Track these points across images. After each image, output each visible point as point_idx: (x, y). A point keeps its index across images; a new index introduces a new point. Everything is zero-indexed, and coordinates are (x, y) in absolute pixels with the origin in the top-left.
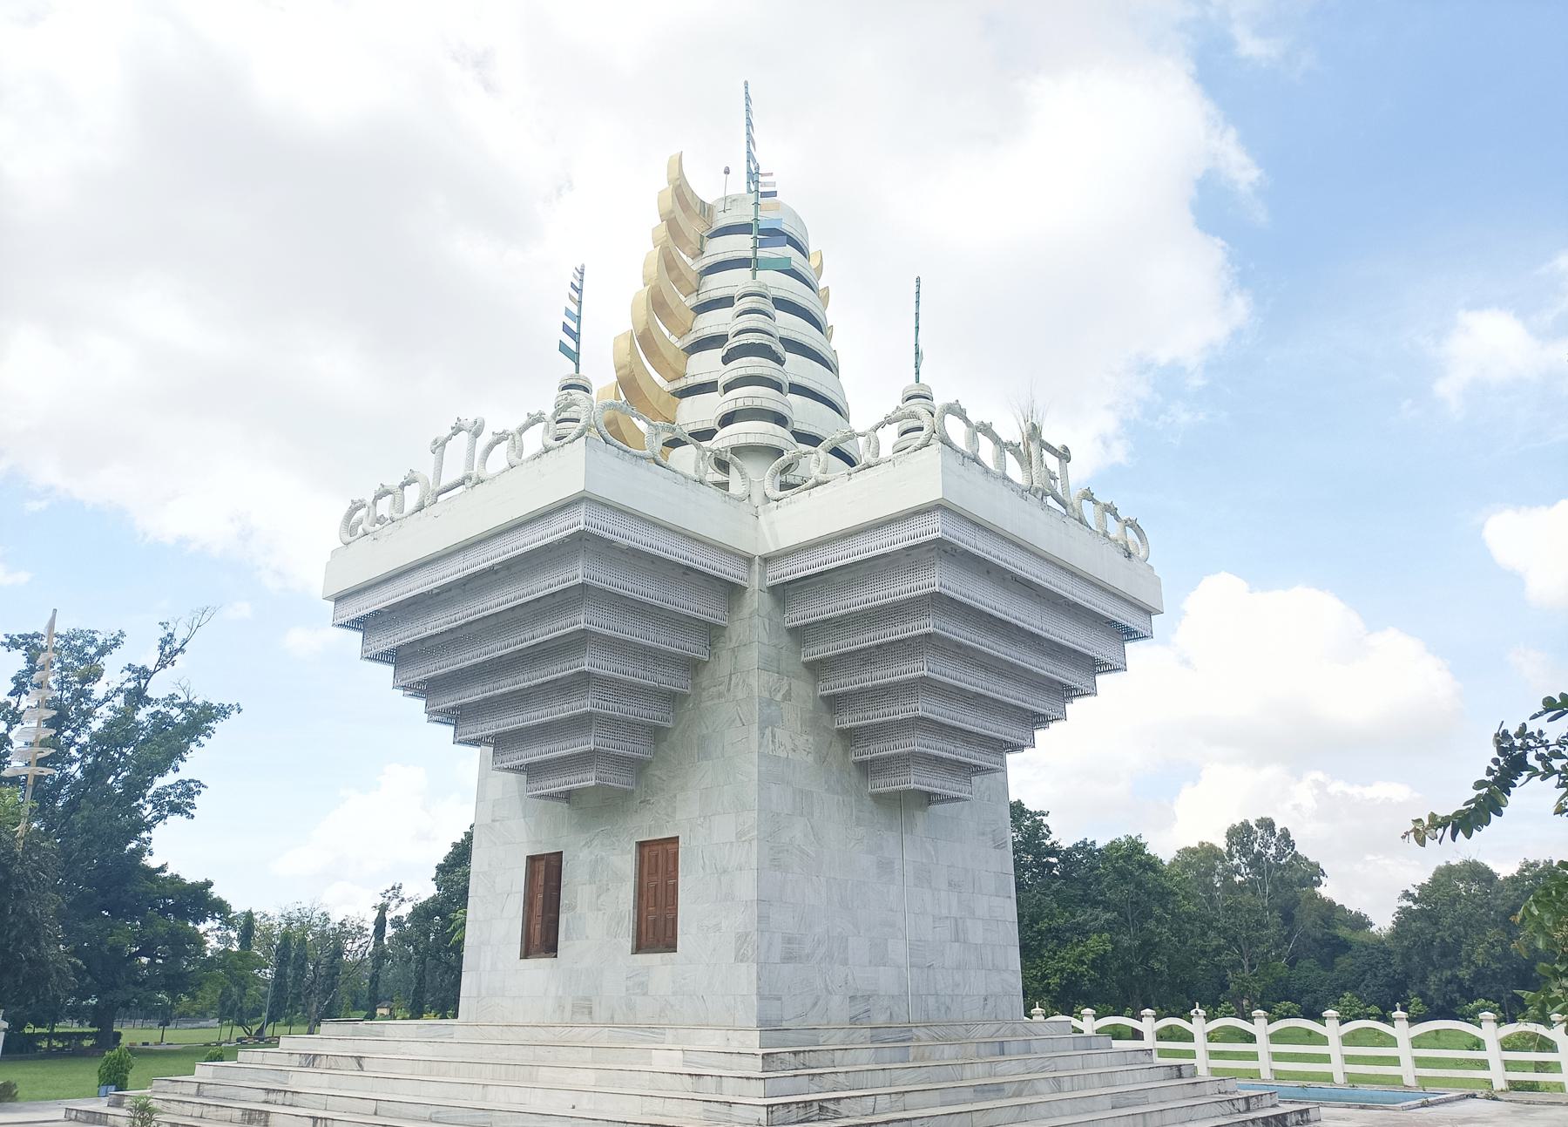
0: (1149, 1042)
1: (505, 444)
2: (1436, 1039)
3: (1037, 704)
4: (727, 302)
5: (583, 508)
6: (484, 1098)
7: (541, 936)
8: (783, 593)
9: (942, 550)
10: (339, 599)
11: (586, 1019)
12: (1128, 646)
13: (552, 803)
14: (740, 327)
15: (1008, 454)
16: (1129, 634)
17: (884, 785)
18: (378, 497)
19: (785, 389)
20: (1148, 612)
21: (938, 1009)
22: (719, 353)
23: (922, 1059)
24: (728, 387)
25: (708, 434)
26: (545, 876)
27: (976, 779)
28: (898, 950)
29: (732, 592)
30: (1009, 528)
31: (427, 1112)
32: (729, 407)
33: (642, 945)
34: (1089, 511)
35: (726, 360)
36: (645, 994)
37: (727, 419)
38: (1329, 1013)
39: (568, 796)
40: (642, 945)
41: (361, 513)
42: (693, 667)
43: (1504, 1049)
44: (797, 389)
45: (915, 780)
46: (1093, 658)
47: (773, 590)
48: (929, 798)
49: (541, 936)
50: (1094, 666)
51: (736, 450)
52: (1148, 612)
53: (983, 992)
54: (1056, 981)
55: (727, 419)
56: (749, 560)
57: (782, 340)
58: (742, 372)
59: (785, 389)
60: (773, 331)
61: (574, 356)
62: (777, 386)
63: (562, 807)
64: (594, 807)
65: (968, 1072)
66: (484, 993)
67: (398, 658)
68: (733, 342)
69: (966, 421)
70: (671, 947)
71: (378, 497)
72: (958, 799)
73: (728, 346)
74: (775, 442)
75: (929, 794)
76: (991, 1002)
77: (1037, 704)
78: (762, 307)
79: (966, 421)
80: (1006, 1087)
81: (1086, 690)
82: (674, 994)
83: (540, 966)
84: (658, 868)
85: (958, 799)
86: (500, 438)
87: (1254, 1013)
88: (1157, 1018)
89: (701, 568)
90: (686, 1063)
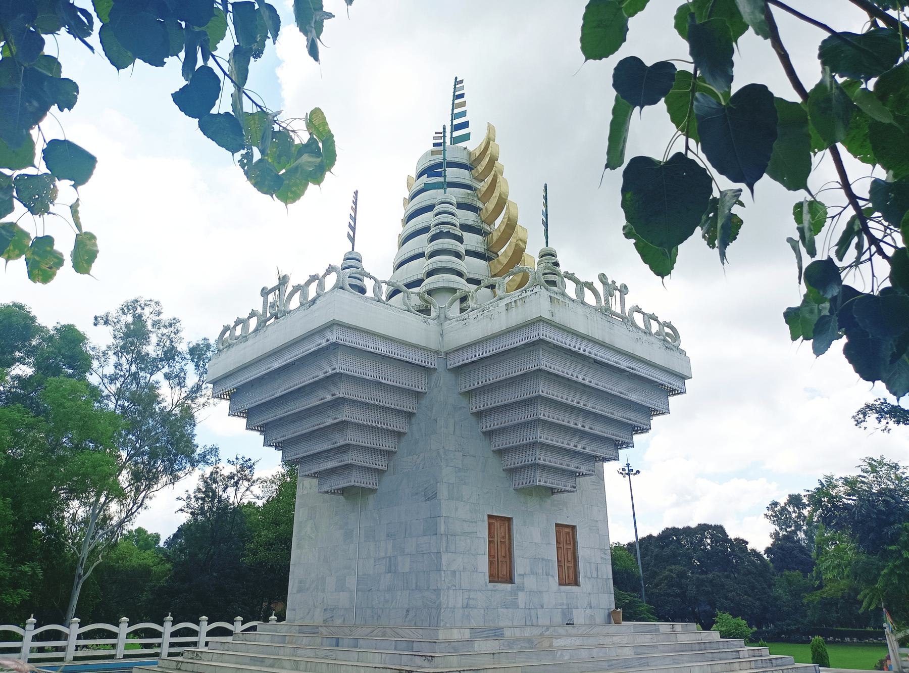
3: (618, 434)
4: (430, 208)
8: (458, 370)
12: (670, 398)
13: (323, 495)
14: (437, 222)
15: (586, 289)
16: (673, 392)
21: (373, 617)
22: (426, 237)
23: (292, 643)
24: (433, 255)
27: (578, 479)
28: (352, 582)
29: (427, 371)
30: (480, 336)
32: (431, 267)
33: (494, 578)
37: (430, 274)
39: (344, 491)
40: (494, 578)
44: (469, 253)
45: (542, 479)
46: (649, 408)
50: (651, 412)
52: (683, 378)
53: (406, 606)
55: (430, 274)
61: (352, 239)
62: (458, 255)
65: (281, 651)
72: (568, 491)
73: (431, 234)
75: (552, 489)
76: (412, 614)
77: (618, 434)
78: (451, 210)
80: (266, 660)
81: (645, 427)
85: (568, 491)
86: (296, 289)
90: (635, 653)
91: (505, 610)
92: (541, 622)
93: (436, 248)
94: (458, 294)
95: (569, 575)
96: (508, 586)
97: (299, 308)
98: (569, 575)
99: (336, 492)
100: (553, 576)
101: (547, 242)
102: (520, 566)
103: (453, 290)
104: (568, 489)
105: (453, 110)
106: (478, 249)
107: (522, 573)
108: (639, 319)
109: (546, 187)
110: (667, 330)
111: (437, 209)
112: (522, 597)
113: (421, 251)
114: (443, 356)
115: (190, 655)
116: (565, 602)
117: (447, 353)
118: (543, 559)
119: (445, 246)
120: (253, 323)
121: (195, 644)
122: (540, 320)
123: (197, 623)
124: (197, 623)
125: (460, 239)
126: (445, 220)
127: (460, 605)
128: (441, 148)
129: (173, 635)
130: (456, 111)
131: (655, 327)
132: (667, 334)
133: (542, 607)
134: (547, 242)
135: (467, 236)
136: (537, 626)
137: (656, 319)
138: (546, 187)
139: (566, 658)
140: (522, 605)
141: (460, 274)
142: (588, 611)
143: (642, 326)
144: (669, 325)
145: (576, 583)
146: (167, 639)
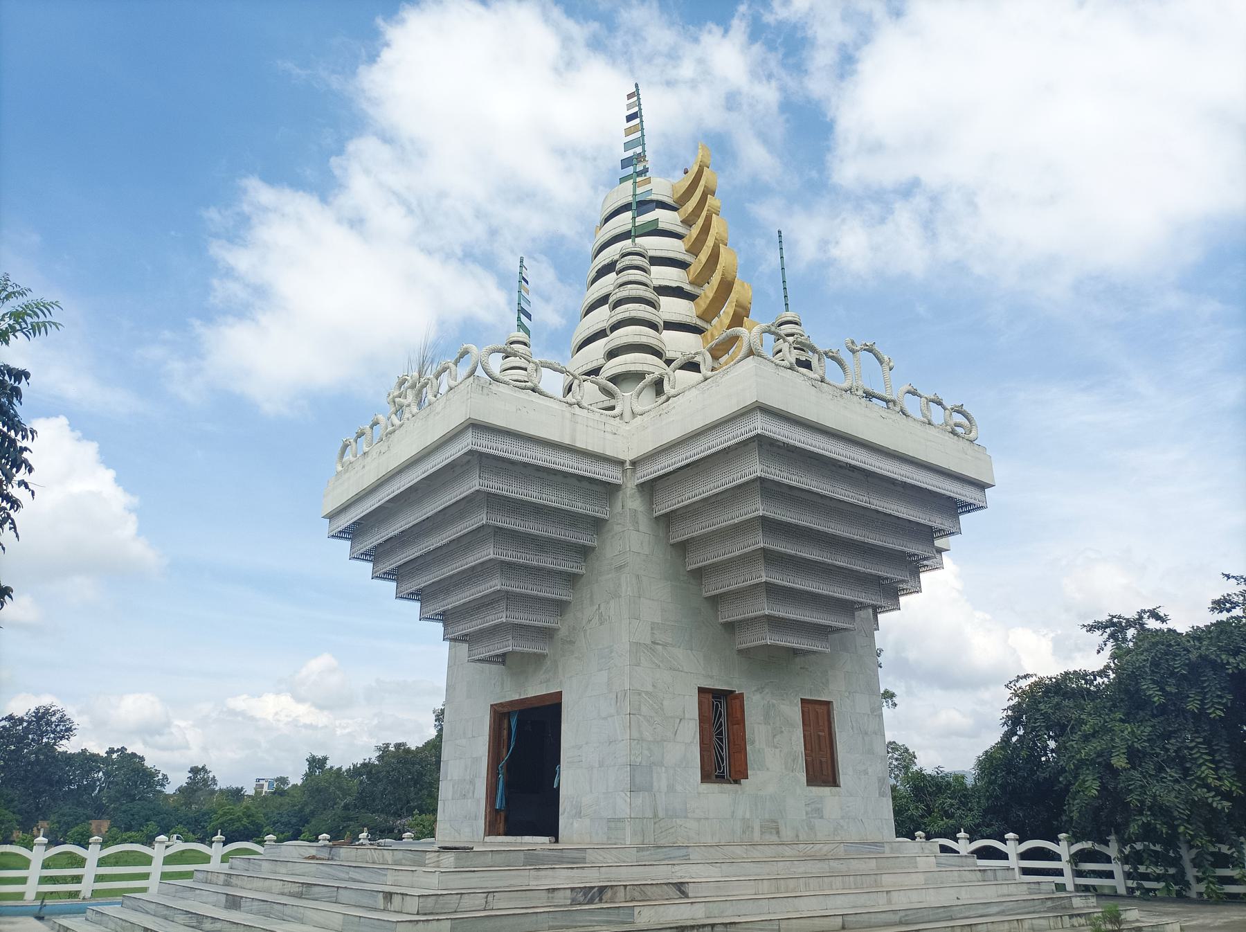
0: (1014, 862)
2: (116, 860)
5: (470, 433)
6: (889, 902)
8: (650, 489)
9: (478, 460)
10: (332, 516)
11: (774, 838)
13: (486, 666)
16: (968, 507)
20: (982, 486)
25: (595, 372)
29: (609, 490)
31: (896, 918)
34: (911, 404)
36: (822, 817)
38: (1062, 836)
39: (502, 659)
42: (584, 552)
44: (670, 326)
47: (641, 487)
52: (982, 486)
57: (655, 289)
58: (627, 315)
59: (661, 328)
60: (648, 282)
62: (653, 326)
63: (495, 668)
64: (774, 663)
66: (661, 814)
67: (374, 555)
70: (706, 778)
82: (842, 818)
83: (719, 796)
87: (1006, 836)
88: (1020, 841)
93: (620, 317)
94: (648, 378)
95: (822, 769)
98: (822, 769)
99: (502, 659)
103: (639, 376)
105: (643, 135)
106: (687, 320)
110: (959, 418)
111: (618, 266)
114: (628, 466)
117: (634, 463)
119: (633, 314)
122: (761, 408)
124: (1106, 843)
125: (653, 304)
126: (632, 278)
129: (102, 862)
130: (639, 134)
132: (957, 425)
135: (664, 301)
141: (658, 353)
143: (919, 417)
144: (959, 411)
145: (833, 781)
146: (156, 868)
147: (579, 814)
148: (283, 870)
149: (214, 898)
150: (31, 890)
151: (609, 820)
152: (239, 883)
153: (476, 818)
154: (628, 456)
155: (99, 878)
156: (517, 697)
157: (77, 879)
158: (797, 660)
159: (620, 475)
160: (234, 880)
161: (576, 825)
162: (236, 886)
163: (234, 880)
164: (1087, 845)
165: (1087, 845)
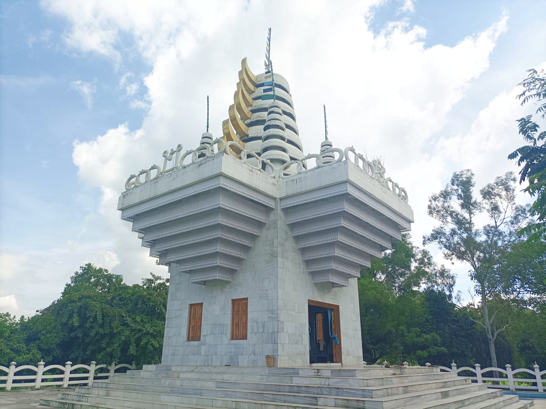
0: (479, 378)
1: (191, 154)
7: (194, 333)
8: (287, 211)
17: (320, 279)
18: (141, 173)
19: (286, 141)
22: (263, 127)
26: (196, 310)
27: (350, 279)
29: (268, 210)
35: (265, 129)
39: (204, 283)
41: (133, 180)
42: (253, 237)
43: (483, 377)
44: (290, 142)
48: (334, 285)
49: (194, 333)
51: (272, 160)
52: (410, 222)
54: (268, 357)
56: (274, 199)
67: (144, 231)
68: (267, 123)
69: (355, 153)
71: (141, 173)
72: (343, 286)
73: (266, 124)
74: (284, 158)
75: (333, 283)
79: (355, 153)
84: (240, 307)
85: (343, 286)
89: (174, 218)
91: (193, 357)
92: (214, 364)
96: (196, 343)
97: (190, 164)
100: (226, 334)
101: (207, 129)
102: (205, 329)
104: (344, 284)
107: (205, 334)
108: (390, 184)
109: (208, 98)
110: (403, 193)
112: (203, 349)
113: (259, 135)
115: (395, 391)
116: (233, 351)
117: (281, 199)
118: (220, 324)
120: (154, 174)
121: (33, 381)
123: (64, 365)
127: (170, 354)
128: (271, 74)
131: (397, 191)
133: (216, 354)
134: (207, 129)
136: (212, 366)
137: (398, 187)
138: (208, 98)
139: (167, 384)
140: (203, 353)
142: (252, 357)
147: (348, 355)
148: (406, 381)
149: (435, 396)
150: (9, 385)
151: (358, 357)
152: (414, 389)
153: (305, 354)
154: (278, 196)
155: (71, 379)
156: (321, 301)
157: (61, 379)
158: (334, 289)
159: (274, 204)
160: (410, 389)
161: (348, 358)
162: (413, 391)
163: (410, 389)
164: (104, 366)
165: (104, 366)
